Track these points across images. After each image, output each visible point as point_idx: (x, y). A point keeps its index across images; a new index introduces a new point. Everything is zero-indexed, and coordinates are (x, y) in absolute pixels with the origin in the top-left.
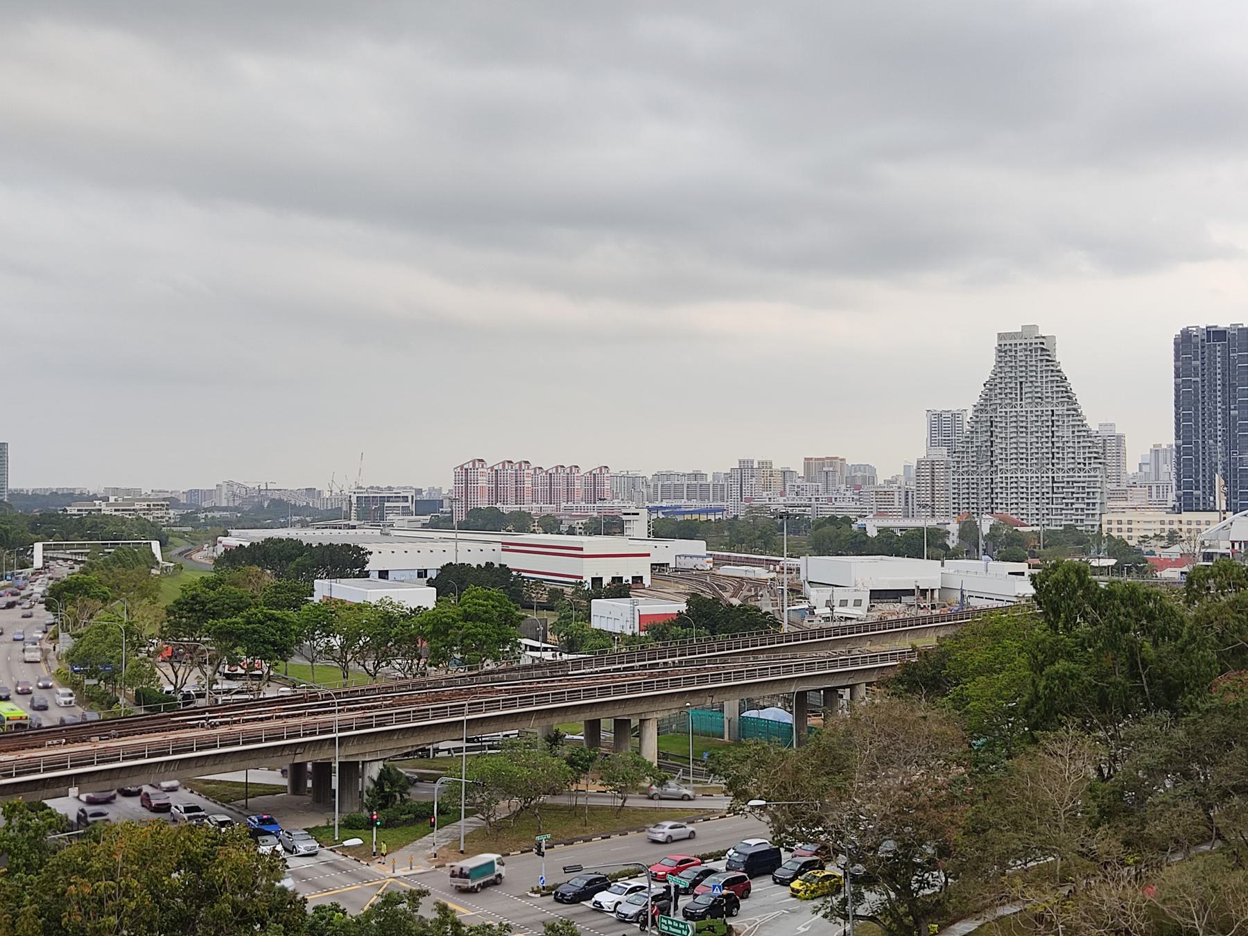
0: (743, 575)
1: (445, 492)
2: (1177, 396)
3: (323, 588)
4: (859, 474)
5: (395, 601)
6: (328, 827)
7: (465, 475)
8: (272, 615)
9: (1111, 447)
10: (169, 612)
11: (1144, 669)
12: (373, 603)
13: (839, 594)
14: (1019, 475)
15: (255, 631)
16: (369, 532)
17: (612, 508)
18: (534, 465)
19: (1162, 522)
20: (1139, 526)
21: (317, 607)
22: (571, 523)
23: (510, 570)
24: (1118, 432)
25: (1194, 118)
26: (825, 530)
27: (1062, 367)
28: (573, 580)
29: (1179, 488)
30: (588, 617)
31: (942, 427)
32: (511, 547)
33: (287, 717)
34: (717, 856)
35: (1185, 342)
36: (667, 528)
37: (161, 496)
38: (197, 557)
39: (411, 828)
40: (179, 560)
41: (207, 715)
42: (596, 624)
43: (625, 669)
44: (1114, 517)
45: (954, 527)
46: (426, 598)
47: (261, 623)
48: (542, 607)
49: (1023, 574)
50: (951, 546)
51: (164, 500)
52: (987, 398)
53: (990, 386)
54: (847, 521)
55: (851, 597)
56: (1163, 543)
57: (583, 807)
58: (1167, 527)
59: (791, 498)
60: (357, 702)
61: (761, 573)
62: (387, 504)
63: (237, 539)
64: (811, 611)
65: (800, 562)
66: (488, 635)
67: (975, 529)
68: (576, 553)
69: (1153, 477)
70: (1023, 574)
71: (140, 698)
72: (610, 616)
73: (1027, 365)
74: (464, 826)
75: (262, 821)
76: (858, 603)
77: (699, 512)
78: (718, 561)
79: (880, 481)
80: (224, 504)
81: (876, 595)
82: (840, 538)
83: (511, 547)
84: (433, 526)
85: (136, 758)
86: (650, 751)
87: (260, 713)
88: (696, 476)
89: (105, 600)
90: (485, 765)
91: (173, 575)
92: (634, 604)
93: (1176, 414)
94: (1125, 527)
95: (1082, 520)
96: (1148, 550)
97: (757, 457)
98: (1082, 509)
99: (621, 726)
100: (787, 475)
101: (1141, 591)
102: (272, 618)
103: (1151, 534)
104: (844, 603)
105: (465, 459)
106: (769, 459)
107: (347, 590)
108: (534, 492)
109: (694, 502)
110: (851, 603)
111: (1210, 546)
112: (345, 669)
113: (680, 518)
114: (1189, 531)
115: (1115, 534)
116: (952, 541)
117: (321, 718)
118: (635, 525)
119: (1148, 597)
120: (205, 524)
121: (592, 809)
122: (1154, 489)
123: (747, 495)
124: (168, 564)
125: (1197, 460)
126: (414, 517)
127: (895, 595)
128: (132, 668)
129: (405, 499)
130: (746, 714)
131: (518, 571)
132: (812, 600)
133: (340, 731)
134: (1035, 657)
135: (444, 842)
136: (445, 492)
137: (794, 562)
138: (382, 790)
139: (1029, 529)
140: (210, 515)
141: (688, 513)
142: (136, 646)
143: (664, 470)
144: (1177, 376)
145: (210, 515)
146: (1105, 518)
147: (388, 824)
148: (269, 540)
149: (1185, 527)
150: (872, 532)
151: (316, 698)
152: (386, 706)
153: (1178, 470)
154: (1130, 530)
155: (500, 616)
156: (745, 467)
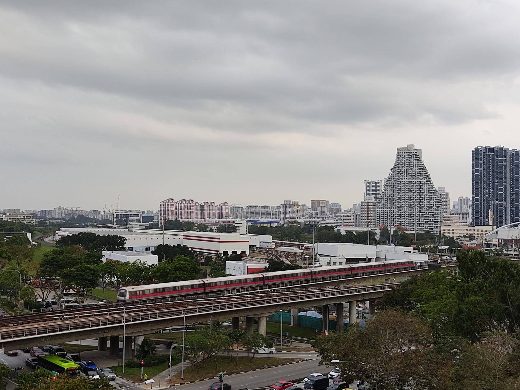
0: (289, 251)
1: (154, 213)
2: (473, 176)
3: (108, 255)
4: (334, 207)
5: (142, 261)
7: (165, 205)
8: (89, 267)
10: (41, 265)
12: (132, 262)
14: (406, 209)
15: (81, 275)
16: (123, 230)
17: (229, 221)
18: (195, 201)
19: (467, 230)
20: (457, 232)
21: (106, 263)
22: (211, 227)
24: (446, 191)
25: (484, 58)
26: (323, 231)
27: (424, 163)
28: (216, 252)
29: (473, 216)
30: (224, 269)
31: (371, 188)
32: (187, 237)
33: (100, 315)
34: (299, 381)
35: (476, 153)
36: (254, 230)
37: (29, 212)
38: (47, 240)
39: (157, 367)
40: (40, 241)
41: (63, 314)
43: (250, 294)
45: (378, 231)
46: (152, 260)
47: (82, 270)
48: (202, 264)
49: (410, 252)
50: (377, 239)
51: (31, 214)
52: (392, 176)
53: (394, 170)
54: (332, 228)
55: (338, 261)
56: (467, 239)
57: (235, 357)
58: (469, 232)
59: (306, 217)
60: (131, 308)
61: (296, 250)
62: (130, 218)
63: (64, 232)
65: (315, 245)
67: (388, 232)
68: (217, 240)
69: (459, 210)
70: (410, 252)
71: (28, 305)
73: (409, 162)
74: (183, 365)
77: (267, 223)
78: (278, 245)
79: (343, 211)
80: (57, 217)
81: (349, 261)
83: (187, 237)
84: (150, 227)
85: (31, 335)
86: (263, 330)
87: (87, 313)
88: (265, 207)
89: (9, 259)
90: (193, 339)
93: (473, 184)
94: (451, 232)
95: (432, 229)
96: (460, 242)
97: (292, 200)
98: (432, 224)
99: (249, 320)
100: (304, 207)
101: (509, 263)
102: (89, 268)
103: (462, 235)
105: (165, 198)
106: (297, 200)
107: (117, 256)
108: (195, 213)
110: (338, 264)
111: (489, 241)
113: (259, 226)
114: (478, 234)
115: (446, 235)
116: (378, 237)
117: (116, 316)
118: (240, 228)
119: (512, 265)
120: (49, 225)
121: (240, 358)
122: (461, 216)
123: (287, 216)
124: (34, 243)
126: (142, 224)
128: (23, 291)
129: (138, 215)
130: (300, 314)
131: (192, 248)
132: (321, 262)
133: (126, 322)
134: (459, 293)
135: (173, 374)
136: (154, 213)
137: (310, 245)
138: (144, 349)
139: (410, 232)
140: (51, 221)
141: (262, 223)
142: (25, 281)
143: (251, 204)
144: (473, 167)
145: (51, 221)
146: (442, 228)
148: (81, 233)
149: (476, 232)
150: (343, 233)
151: (112, 306)
152: (145, 310)
153: (473, 208)
154: (453, 233)
155: (191, 269)
156: (287, 204)
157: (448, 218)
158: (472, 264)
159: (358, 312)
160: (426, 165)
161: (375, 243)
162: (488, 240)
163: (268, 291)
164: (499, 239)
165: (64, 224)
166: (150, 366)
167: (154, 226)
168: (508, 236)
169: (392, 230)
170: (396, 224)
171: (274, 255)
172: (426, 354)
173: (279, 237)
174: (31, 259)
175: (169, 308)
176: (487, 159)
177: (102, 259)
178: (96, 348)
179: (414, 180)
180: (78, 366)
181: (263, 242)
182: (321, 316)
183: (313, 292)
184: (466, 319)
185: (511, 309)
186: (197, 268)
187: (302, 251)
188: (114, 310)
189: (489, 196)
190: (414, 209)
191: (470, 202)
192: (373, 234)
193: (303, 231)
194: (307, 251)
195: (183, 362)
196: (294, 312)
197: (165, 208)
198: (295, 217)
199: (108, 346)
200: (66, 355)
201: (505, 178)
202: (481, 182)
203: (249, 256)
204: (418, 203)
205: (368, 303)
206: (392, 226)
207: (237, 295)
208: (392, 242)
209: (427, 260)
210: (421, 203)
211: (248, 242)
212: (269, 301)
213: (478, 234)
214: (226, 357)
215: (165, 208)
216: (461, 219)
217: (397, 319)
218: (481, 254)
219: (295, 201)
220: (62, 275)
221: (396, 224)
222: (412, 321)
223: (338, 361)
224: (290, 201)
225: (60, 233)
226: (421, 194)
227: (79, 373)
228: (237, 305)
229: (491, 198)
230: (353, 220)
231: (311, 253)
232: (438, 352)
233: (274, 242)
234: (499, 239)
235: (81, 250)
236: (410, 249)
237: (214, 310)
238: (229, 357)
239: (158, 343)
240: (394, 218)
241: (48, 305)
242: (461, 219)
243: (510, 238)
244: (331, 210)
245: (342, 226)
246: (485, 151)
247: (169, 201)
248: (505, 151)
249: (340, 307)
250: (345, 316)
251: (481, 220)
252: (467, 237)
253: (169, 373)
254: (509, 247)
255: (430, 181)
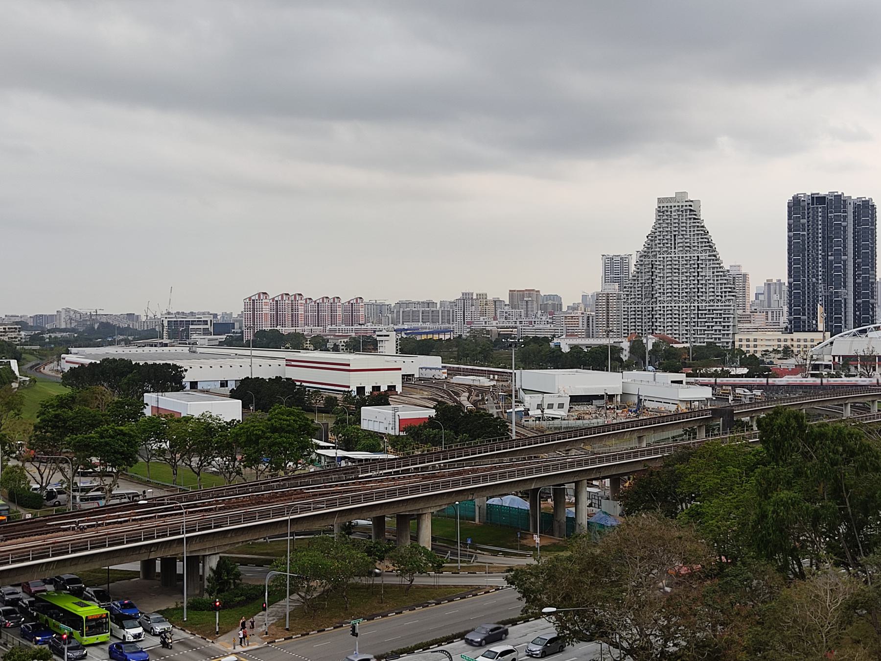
0: (471, 383)
1: (235, 316)
4: (550, 302)
5: (214, 415)
6: (176, 609)
7: (253, 304)
9: (739, 283)
10: (36, 428)
11: (847, 492)
12: (196, 416)
13: (548, 399)
15: (107, 444)
16: (179, 349)
18: (305, 296)
19: (779, 340)
22: (335, 341)
23: (293, 381)
24: (743, 271)
27: (705, 224)
29: (790, 314)
31: (614, 268)
32: (293, 363)
33: (141, 519)
35: (796, 206)
38: (47, 370)
42: (364, 425)
43: (404, 472)
44: (744, 337)
45: (626, 345)
46: (230, 411)
47: (111, 437)
48: (321, 411)
49: (681, 382)
50: (625, 359)
51: (17, 323)
52: (649, 247)
53: (652, 237)
54: (546, 340)
56: (779, 356)
58: (783, 344)
60: (195, 506)
61: (484, 381)
62: (191, 327)
63: (80, 357)
64: (526, 412)
66: (291, 444)
67: (643, 347)
68: (344, 367)
69: (766, 304)
72: (374, 419)
73: (679, 222)
74: (287, 604)
75: (125, 606)
76: (561, 406)
78: (452, 372)
79: (565, 309)
80: (63, 326)
81: (576, 400)
82: (541, 354)
83: (293, 363)
84: (229, 343)
86: (426, 539)
87: (119, 517)
90: (305, 559)
91: (29, 387)
92: (395, 410)
93: (789, 259)
94: (752, 344)
95: (719, 339)
96: (768, 360)
97: (475, 291)
98: (720, 330)
99: (402, 520)
100: (497, 303)
103: (771, 349)
104: (550, 406)
105: (252, 292)
108: (306, 317)
109: (428, 325)
110: (555, 406)
111: (817, 360)
112: (174, 466)
113: (418, 338)
114: (799, 346)
115: (744, 349)
117: (169, 521)
119: (851, 435)
120: (50, 343)
121: (387, 587)
122: (770, 313)
123: (468, 319)
125: (804, 293)
126: (213, 337)
127: (587, 399)
129: (206, 322)
132: (526, 404)
133: (187, 532)
136: (235, 316)
140: (53, 335)
144: (790, 230)
145: (53, 335)
146: (737, 337)
147: (225, 606)
149: (795, 344)
150: (566, 349)
152: (220, 509)
154: (755, 346)
156: (466, 298)
157: (746, 319)
158: (782, 436)
159: (590, 496)
160: (708, 228)
161: (621, 366)
162: (815, 357)
163: (434, 466)
164: (834, 357)
165: (76, 339)
166: (231, 607)
167: (235, 341)
168: (850, 351)
169: (650, 342)
170: (657, 332)
171: (445, 391)
172: (704, 596)
173: (454, 358)
174: (19, 411)
175: (263, 503)
176: (814, 215)
177: (145, 411)
178: (136, 573)
179: (688, 255)
180: (104, 611)
181: (426, 369)
182: (526, 505)
183: (512, 466)
184: (773, 531)
185: (850, 510)
186: (310, 425)
187: (494, 383)
188: (166, 510)
189: (817, 280)
190: (688, 304)
191: (785, 288)
192: (616, 350)
193: (495, 346)
194: (504, 383)
195: (287, 599)
196: (480, 501)
197: (254, 309)
198: (480, 323)
199: (158, 569)
200: (84, 589)
201: (845, 247)
202: (804, 256)
203: (401, 395)
204: (697, 292)
205: (607, 482)
206: (651, 336)
207: (381, 475)
208: (650, 363)
209: (710, 396)
210: (700, 294)
211: (400, 369)
212: (435, 487)
213: (799, 346)
214: (363, 585)
215: (254, 309)
216: (770, 320)
217: (654, 534)
218: (798, 417)
219: (481, 292)
220: (74, 445)
221: (657, 332)
222: (680, 538)
223: (555, 609)
224: (472, 294)
225: (69, 357)
226: (700, 278)
227: (107, 623)
228: (380, 496)
229: (821, 287)
230: (582, 326)
231: (509, 386)
232: (726, 593)
233: (444, 367)
234: (834, 357)
235: (108, 394)
236: (681, 377)
237: (340, 505)
238: (369, 585)
239: (245, 562)
240: (654, 320)
241: (51, 495)
242: (770, 320)
243: (853, 353)
244: (544, 308)
245: (564, 336)
246: (810, 202)
247: (259, 297)
248: (845, 201)
249: (559, 494)
250: (569, 503)
251: (804, 322)
252: (779, 352)
253: (264, 619)
254: (852, 369)
255: (715, 256)
